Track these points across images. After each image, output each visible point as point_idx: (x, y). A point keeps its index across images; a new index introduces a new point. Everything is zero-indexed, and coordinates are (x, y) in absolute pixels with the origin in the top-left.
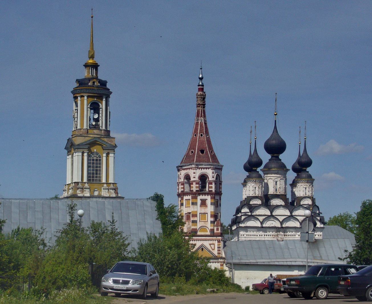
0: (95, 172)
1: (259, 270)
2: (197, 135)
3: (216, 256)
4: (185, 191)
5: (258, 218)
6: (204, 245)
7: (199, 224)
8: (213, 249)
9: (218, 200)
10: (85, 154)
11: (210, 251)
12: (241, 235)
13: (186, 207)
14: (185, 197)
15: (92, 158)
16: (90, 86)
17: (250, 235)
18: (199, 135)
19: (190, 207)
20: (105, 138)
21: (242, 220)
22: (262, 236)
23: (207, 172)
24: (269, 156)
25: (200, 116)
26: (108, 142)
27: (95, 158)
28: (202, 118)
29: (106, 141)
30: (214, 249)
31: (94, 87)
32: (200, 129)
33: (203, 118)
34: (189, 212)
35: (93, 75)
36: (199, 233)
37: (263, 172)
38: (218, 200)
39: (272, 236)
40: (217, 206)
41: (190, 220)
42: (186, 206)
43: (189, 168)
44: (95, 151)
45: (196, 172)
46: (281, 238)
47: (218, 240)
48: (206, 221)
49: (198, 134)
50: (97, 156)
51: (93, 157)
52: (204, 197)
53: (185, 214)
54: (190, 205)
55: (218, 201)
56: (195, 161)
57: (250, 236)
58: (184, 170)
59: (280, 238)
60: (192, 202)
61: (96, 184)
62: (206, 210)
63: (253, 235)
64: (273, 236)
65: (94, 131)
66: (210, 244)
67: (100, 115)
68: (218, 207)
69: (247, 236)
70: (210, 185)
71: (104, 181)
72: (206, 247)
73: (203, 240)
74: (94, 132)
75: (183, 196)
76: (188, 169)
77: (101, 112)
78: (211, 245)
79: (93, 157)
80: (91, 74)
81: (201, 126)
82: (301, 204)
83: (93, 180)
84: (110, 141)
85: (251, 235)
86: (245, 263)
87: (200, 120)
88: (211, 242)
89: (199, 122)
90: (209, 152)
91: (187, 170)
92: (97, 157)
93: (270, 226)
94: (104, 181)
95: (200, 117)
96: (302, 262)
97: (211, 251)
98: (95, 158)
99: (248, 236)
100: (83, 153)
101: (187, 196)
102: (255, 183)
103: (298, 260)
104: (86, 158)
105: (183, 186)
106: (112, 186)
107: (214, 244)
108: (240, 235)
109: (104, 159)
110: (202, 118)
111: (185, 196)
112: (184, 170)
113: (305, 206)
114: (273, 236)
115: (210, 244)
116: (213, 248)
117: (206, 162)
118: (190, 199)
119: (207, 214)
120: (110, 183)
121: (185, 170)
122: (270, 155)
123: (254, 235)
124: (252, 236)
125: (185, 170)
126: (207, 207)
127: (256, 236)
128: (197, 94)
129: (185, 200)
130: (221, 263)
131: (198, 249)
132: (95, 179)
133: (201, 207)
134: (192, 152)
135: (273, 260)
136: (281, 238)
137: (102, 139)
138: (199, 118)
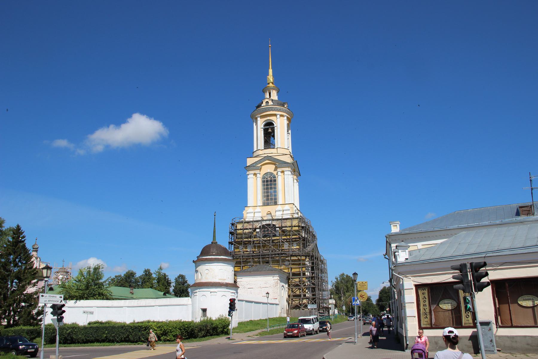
27: (269, 179)
92: (271, 178)
98: (269, 179)
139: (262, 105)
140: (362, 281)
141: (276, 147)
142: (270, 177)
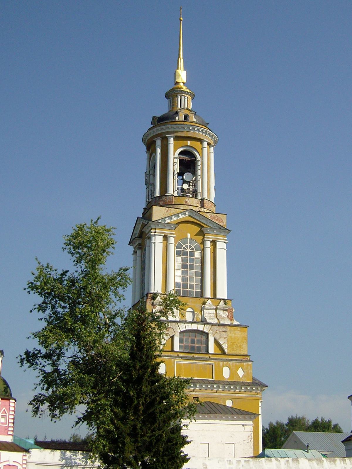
10: (172, 240)
15: (182, 250)
50: (193, 247)
51: (184, 248)
65: (187, 200)
79: (184, 248)
94: (208, 293)
100: (166, 238)
141: (199, 197)
142: (190, 247)
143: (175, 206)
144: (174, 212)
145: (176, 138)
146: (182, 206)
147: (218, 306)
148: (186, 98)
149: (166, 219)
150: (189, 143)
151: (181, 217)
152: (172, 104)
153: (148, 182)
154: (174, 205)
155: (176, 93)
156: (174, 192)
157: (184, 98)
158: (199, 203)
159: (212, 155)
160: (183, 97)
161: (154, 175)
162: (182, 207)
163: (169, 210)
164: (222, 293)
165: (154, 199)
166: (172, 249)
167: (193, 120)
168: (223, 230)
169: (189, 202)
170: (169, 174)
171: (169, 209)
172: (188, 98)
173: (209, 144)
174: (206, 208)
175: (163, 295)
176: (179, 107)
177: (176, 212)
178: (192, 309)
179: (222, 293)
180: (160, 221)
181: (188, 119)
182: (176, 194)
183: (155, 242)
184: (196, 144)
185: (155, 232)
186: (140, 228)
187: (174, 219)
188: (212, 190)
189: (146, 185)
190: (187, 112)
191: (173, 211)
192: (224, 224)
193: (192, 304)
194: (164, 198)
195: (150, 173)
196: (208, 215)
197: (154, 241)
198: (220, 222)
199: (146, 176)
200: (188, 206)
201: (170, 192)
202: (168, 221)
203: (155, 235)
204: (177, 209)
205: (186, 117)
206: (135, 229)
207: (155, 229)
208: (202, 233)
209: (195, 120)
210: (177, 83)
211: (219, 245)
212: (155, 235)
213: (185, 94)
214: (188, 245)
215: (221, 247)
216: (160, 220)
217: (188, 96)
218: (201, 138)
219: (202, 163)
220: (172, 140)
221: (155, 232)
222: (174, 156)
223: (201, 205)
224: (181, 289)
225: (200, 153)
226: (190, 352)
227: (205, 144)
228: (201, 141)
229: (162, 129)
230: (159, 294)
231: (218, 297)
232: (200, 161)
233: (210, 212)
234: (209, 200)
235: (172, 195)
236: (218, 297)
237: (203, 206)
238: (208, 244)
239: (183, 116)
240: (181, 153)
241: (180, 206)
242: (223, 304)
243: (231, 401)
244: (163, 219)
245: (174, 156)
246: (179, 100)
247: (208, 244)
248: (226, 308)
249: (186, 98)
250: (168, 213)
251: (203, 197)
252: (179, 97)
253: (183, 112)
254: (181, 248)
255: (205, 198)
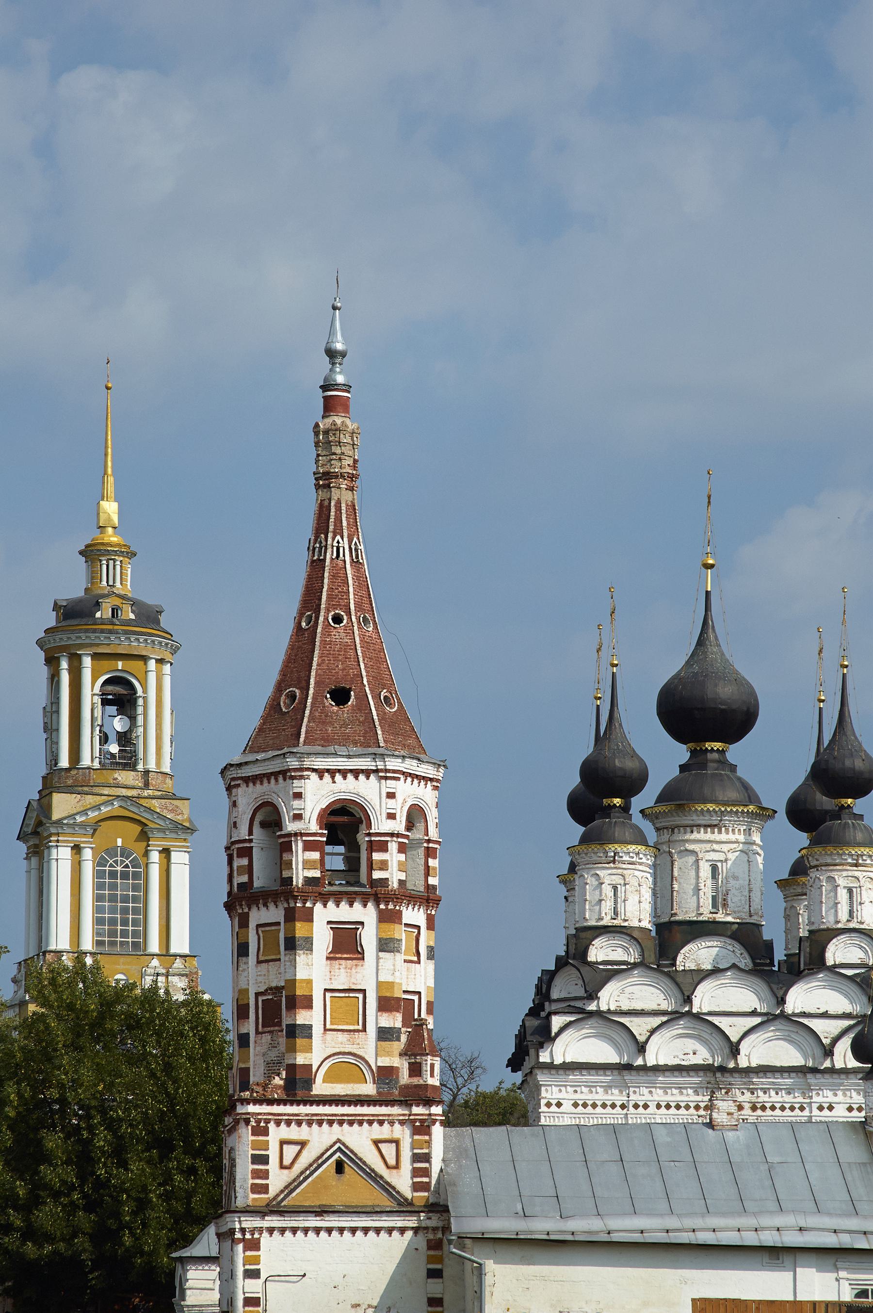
0: (119, 916)
1: (611, 1266)
2: (317, 618)
3: (406, 1199)
4: (257, 884)
5: (628, 1024)
6: (344, 1144)
7: (324, 1041)
8: (388, 1167)
9: (418, 927)
10: (87, 854)
11: (374, 1177)
12: (549, 1105)
13: (259, 962)
14: (258, 916)
15: (107, 868)
16: (102, 622)
17: (590, 1103)
18: (326, 619)
19: (279, 960)
20: (154, 801)
21: (553, 1034)
22: (646, 1106)
23: (363, 792)
24: (681, 753)
25: (331, 528)
26: (165, 813)
27: (119, 868)
28: (338, 537)
29: (158, 811)
30: (397, 1166)
31: (113, 624)
32: (330, 589)
33: (346, 539)
34: (274, 985)
35: (113, 586)
36: (320, 1088)
37: (654, 824)
38: (418, 927)
39: (692, 1111)
40: (415, 959)
41: (279, 1024)
42: (261, 958)
43: (272, 774)
44: (119, 842)
45: (303, 791)
46: (728, 1114)
47: (415, 1121)
48: (358, 1031)
49: (322, 614)
50: (127, 862)
51: (111, 866)
52: (344, 912)
53: (257, 995)
54: (279, 953)
55: (419, 933)
56: (302, 739)
57: (589, 1109)
58: (251, 785)
59: (725, 1116)
60: (286, 938)
61: (122, 959)
62: (359, 976)
63: (604, 1106)
64: (697, 1108)
65: (116, 776)
66: (376, 1143)
67: (140, 720)
68: (419, 962)
69: (575, 1111)
70: (376, 856)
71: (154, 946)
72: (355, 1155)
73: (341, 1123)
74: (115, 779)
75: (246, 910)
76: (268, 776)
77: (140, 710)
78: (382, 1146)
79: (111, 866)
80: (107, 582)
81: (333, 577)
82: (830, 962)
83: (113, 944)
84: (172, 811)
85: (594, 1106)
86: (545, 1237)
87: (329, 547)
88: (384, 1132)
89: (324, 560)
90: (377, 697)
91: (265, 781)
92: (127, 866)
93: (683, 1063)
94: (154, 946)
95: (330, 535)
96: (865, 1233)
97: (381, 1177)
99: (580, 1108)
100: (77, 849)
101: (265, 905)
102: (612, 865)
103: (812, 1221)
104: (88, 869)
105: (245, 862)
106: (178, 964)
107: (397, 1142)
108: (543, 1102)
109: (155, 872)
110: (338, 537)
111: (254, 909)
112: (251, 785)
113: (849, 972)
114: (697, 1108)
115: (376, 1143)
116: (392, 1161)
117: (355, 744)
118: (278, 924)
119: (360, 996)
120: (175, 956)
121: (254, 784)
122: (684, 747)
123: (609, 1103)
124: (599, 1110)
125: (254, 784)
126: (360, 963)
127: (618, 1108)
128: (317, 425)
129: (258, 926)
130: (431, 1236)
131: (317, 1163)
132: (106, 939)
133: (336, 959)
134: (292, 697)
135: (689, 1223)
136: (728, 1114)
137: (142, 802)
138: (326, 540)
139: (98, 615)
140: (836, 1228)
141: (140, 767)
143: (96, 790)
144: (91, 801)
145: (95, 656)
146: (107, 788)
147: (170, 970)
148: (118, 563)
149: (77, 817)
150: (120, 665)
151: (104, 809)
152: (93, 576)
153: (50, 727)
154: (92, 786)
155: (98, 553)
156: (92, 761)
157: (114, 562)
158: (140, 778)
159: (167, 681)
160: (111, 562)
161: (58, 712)
162: (106, 791)
163: (83, 798)
164: (180, 943)
165: (57, 771)
166: (88, 869)
167: (129, 616)
168: (185, 830)
169: (120, 778)
170: (84, 727)
171: (82, 797)
172: (121, 561)
173: (160, 661)
174: (152, 788)
175: (72, 954)
176: (104, 583)
177: (95, 801)
178: (124, 974)
179: (180, 943)
180: (65, 822)
181: (119, 615)
182: (96, 765)
183: (57, 859)
184: (135, 666)
185: (58, 841)
186: (34, 818)
187: (92, 814)
188: (167, 749)
189: (45, 732)
190: (117, 602)
191: (90, 800)
192: (185, 817)
193: (124, 967)
194: (74, 772)
195: (53, 710)
196: (156, 804)
197: (56, 858)
198: (178, 815)
199: (45, 716)
200: (117, 788)
201: (86, 760)
202: (79, 819)
203: (57, 846)
204: (97, 796)
205: (115, 611)
206: (29, 810)
207: (58, 834)
208: (144, 836)
209: (132, 616)
210: (102, 528)
211: (175, 856)
212: (57, 846)
213: (115, 556)
214: (119, 859)
215: (180, 859)
216: (65, 818)
217: (121, 558)
218: (144, 653)
219: (145, 699)
220: (87, 661)
221: (58, 841)
222: (92, 691)
223: (145, 784)
224: (106, 939)
225: (143, 682)
226: (388, 839)
227: (152, 664)
228: (144, 659)
229: (69, 638)
230: (65, 952)
231: (173, 951)
232: (141, 697)
233: (160, 793)
234: (158, 771)
235: (89, 768)
236: (173, 951)
237: (147, 785)
238: (155, 856)
239: (110, 609)
240: (107, 682)
241: (104, 789)
242: (180, 964)
243: (837, 1045)
244: (72, 816)
245: (92, 691)
246: (104, 567)
247: (155, 856)
248: (184, 972)
249: (118, 563)
250: (80, 803)
251: (147, 767)
252: (104, 562)
253: (109, 602)
254: (106, 867)
255: (150, 770)
